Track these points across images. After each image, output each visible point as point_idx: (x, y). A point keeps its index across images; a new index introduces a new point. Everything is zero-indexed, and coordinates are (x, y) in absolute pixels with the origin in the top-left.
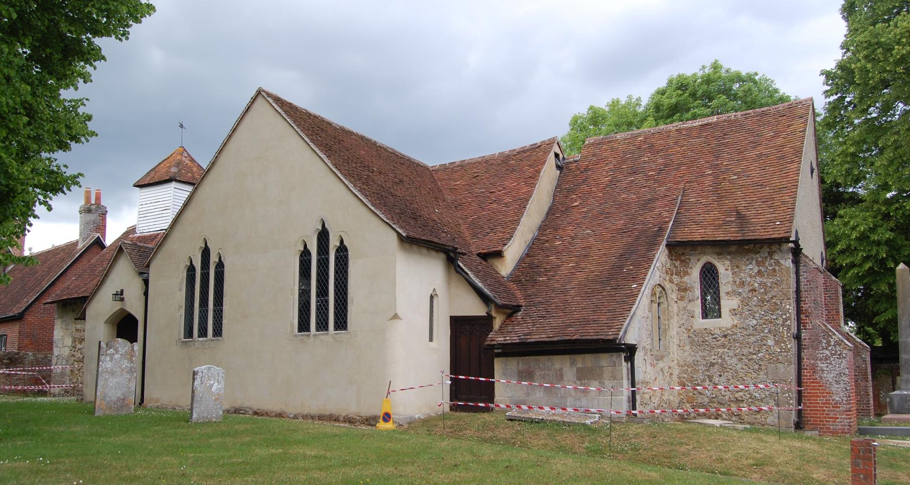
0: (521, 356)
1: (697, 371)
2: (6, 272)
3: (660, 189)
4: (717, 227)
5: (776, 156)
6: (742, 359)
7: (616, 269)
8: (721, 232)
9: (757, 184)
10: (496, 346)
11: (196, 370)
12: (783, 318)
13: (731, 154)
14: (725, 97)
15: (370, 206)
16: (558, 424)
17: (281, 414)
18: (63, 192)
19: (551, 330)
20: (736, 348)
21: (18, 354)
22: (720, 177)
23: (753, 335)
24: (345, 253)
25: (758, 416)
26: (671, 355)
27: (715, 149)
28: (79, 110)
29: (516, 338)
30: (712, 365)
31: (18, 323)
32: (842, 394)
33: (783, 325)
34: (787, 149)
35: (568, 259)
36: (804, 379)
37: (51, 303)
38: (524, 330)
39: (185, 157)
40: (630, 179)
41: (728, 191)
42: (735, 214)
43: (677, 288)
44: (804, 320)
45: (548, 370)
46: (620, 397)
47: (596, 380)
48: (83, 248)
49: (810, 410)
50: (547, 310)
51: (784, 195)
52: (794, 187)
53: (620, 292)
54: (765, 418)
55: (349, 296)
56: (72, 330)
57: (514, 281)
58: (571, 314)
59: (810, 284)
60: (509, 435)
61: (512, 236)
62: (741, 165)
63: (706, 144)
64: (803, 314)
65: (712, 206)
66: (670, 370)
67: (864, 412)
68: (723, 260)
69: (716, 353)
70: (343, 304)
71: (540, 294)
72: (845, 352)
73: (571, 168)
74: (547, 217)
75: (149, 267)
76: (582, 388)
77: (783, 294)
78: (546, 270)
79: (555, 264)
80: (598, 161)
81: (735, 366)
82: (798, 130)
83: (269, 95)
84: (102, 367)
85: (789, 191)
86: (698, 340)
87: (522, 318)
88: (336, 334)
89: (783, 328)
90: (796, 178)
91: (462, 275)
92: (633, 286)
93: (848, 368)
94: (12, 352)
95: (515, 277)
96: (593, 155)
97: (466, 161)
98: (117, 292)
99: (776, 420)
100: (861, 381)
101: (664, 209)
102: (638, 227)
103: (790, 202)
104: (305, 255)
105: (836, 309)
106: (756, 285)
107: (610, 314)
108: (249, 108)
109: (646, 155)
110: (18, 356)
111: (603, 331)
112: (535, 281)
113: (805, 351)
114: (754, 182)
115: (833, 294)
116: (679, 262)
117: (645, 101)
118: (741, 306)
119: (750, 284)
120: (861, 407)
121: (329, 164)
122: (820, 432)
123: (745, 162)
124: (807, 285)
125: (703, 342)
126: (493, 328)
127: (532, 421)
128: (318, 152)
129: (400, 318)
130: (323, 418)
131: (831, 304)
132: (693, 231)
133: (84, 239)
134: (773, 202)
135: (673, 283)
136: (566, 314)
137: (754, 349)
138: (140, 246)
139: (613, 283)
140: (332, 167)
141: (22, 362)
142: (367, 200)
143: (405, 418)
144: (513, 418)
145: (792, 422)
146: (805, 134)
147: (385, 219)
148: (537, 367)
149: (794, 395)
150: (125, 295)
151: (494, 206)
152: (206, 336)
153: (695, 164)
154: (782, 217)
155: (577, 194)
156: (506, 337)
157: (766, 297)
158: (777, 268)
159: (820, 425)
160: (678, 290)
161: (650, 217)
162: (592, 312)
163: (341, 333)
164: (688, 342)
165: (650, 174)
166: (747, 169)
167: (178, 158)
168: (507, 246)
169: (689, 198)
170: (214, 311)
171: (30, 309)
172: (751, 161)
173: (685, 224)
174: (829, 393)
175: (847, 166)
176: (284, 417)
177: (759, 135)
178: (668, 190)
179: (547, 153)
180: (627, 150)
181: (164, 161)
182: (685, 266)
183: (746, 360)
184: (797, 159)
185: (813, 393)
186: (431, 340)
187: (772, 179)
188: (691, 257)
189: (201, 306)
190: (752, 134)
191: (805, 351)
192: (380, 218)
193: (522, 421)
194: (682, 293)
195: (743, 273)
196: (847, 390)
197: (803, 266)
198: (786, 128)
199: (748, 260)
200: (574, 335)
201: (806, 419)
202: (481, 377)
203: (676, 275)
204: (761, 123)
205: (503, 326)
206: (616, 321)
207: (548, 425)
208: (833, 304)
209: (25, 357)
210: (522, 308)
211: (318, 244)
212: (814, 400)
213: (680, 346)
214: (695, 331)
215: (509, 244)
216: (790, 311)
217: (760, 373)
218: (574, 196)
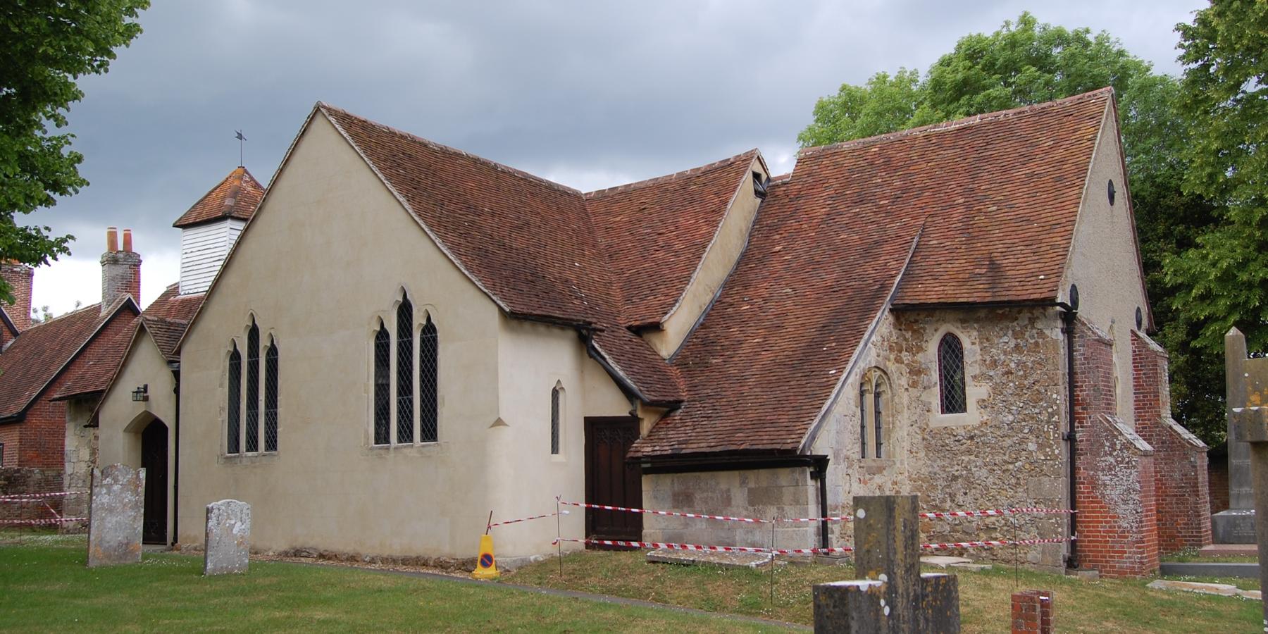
0: (677, 473)
1: (934, 487)
3: (892, 225)
5: (1052, 176)
6: (994, 471)
7: (815, 345)
8: (965, 291)
9: (1022, 219)
10: (642, 459)
11: (210, 506)
12: (1048, 412)
13: (993, 174)
14: (1034, 69)
15: (463, 270)
16: (713, 567)
17: (354, 557)
18: (46, 263)
19: (714, 437)
20: (987, 454)
21: (18, 471)
22: (974, 209)
23: (1009, 436)
24: (434, 335)
26: (898, 464)
27: (973, 166)
28: (62, 151)
29: (667, 448)
30: (955, 478)
31: (18, 427)
32: (1131, 518)
33: (1048, 422)
34: (1068, 166)
35: (755, 331)
36: (1081, 498)
37: (60, 399)
38: (680, 435)
39: (246, 182)
40: (854, 211)
41: (983, 229)
42: (988, 263)
43: (908, 370)
44: (1081, 413)
45: (711, 492)
46: (805, 529)
47: (774, 505)
48: (108, 316)
49: (1088, 540)
50: (715, 408)
51: (1056, 235)
52: (1070, 223)
53: (813, 381)
54: (1025, 553)
55: (439, 395)
56: (89, 438)
57: (679, 365)
58: (745, 412)
59: (1088, 363)
60: (644, 584)
61: (676, 301)
62: (1005, 190)
63: (962, 158)
64: (1079, 405)
65: (958, 251)
66: (895, 487)
67: (1193, 540)
69: (960, 462)
70: (431, 405)
71: (710, 384)
72: (1135, 459)
73: (777, 194)
74: (736, 269)
76: (735, 519)
77: (1048, 378)
78: (724, 347)
79: (737, 339)
80: (814, 183)
81: (985, 480)
82: (1085, 138)
83: (329, 110)
84: (96, 503)
85: (1063, 229)
86: (936, 444)
87: (681, 419)
88: (423, 446)
89: (1048, 426)
90: (1075, 209)
91: (597, 360)
92: (830, 372)
93: (1139, 482)
94: (10, 468)
95: (680, 360)
96: (809, 175)
97: (632, 186)
98: (138, 388)
99: (1040, 556)
100: (1189, 495)
101: (892, 257)
102: (854, 283)
103: (1062, 246)
104: (382, 337)
105: (1154, 392)
106: (1013, 365)
107: (794, 412)
108: (305, 130)
109: (879, 174)
110: (18, 474)
111: (780, 437)
112: (707, 365)
113: (1082, 458)
114: (1018, 216)
115: (1151, 369)
116: (910, 333)
117: (923, 77)
118: (992, 395)
119: (1005, 364)
120: (1189, 532)
121: (410, 211)
122: (1101, 572)
123: (1010, 186)
124: (1084, 364)
125: (943, 446)
126: (640, 434)
127: (680, 563)
128: (396, 193)
129: (505, 424)
130: (408, 562)
131: (1147, 385)
132: (928, 289)
133: (109, 303)
134: (1039, 245)
135: (902, 363)
136: (738, 413)
137: (1010, 457)
138: (169, 323)
139: (806, 367)
140: (413, 214)
141: (24, 483)
142: (459, 262)
143: (514, 561)
144: (656, 560)
145: (1061, 558)
146: (1094, 143)
147: (482, 288)
148: (697, 487)
149: (1066, 520)
151: (661, 254)
152: (257, 450)
153: (943, 188)
154: (1048, 268)
155: (781, 234)
156: (655, 446)
157: (1026, 382)
158: (1040, 341)
159: (1102, 561)
160: (909, 373)
161: (871, 270)
162: (772, 410)
163: (430, 445)
164: (922, 446)
165: (881, 203)
166: (1011, 196)
167: (235, 183)
169: (929, 239)
170: (267, 414)
172: (1019, 184)
173: (919, 279)
174: (1114, 517)
175: (1208, 170)
176: (358, 561)
178: (902, 228)
179: (740, 173)
180: (854, 167)
181: (216, 189)
182: (918, 338)
183: (999, 472)
184: (1078, 182)
185: (1093, 517)
186: (555, 449)
187: (1043, 212)
188: (926, 326)
189: (249, 407)
190: (1024, 143)
191: (1082, 458)
192: (477, 286)
193: (668, 563)
194: (915, 377)
195: (995, 348)
196: (1137, 512)
197: (1079, 337)
198: (1071, 135)
199: (1001, 329)
200: (742, 444)
201: (1083, 554)
202: (607, 505)
203: (906, 351)
204: (1038, 127)
205: (655, 430)
206: (799, 424)
207: (699, 569)
208: (1151, 385)
209: (29, 475)
210: (682, 404)
212: (1093, 527)
213: (912, 453)
214: (931, 431)
215: (672, 312)
216: (1058, 402)
217: (1019, 490)
218: (777, 237)
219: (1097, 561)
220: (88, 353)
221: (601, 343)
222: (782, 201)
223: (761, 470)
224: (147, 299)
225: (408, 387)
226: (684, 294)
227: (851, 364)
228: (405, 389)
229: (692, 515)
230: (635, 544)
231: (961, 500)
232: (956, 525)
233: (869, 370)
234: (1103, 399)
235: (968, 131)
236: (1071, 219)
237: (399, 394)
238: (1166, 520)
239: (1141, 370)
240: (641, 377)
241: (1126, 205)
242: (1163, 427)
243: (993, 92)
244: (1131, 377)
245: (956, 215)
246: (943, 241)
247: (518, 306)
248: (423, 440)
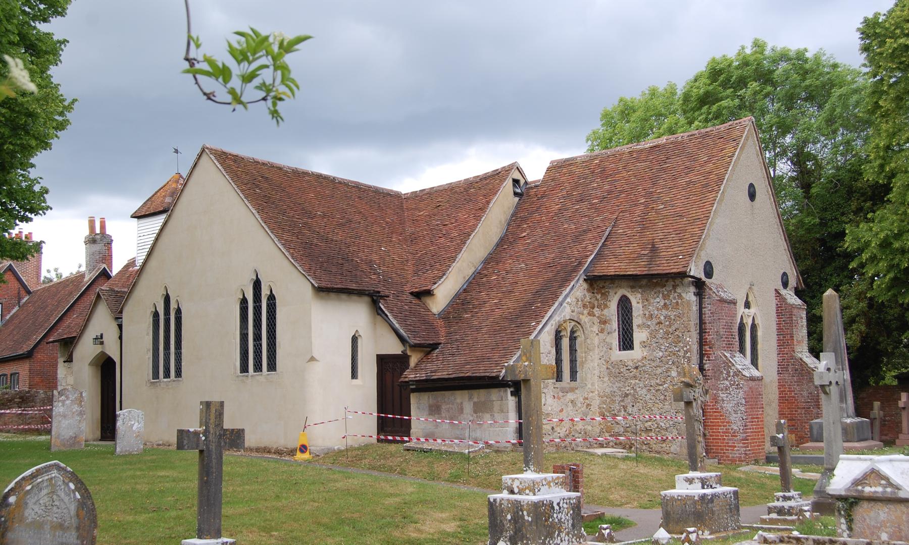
0: (434, 391)
1: (614, 401)
2: (21, 304)
4: (631, 261)
8: (632, 266)
15: (291, 259)
16: (440, 452)
18: (27, 259)
21: (28, 392)
25: (664, 445)
26: (589, 386)
30: (627, 395)
37: (54, 342)
40: (576, 207)
41: (652, 222)
42: (650, 246)
51: (696, 226)
52: (706, 218)
59: (713, 316)
61: (444, 274)
68: (635, 293)
75: (122, 313)
85: (700, 223)
88: (268, 375)
95: (445, 315)
96: (553, 180)
99: (678, 449)
100: (813, 408)
104: (244, 302)
105: (790, 334)
106: (662, 318)
108: (196, 164)
113: (709, 381)
115: (788, 318)
116: (600, 295)
124: (710, 317)
127: (425, 451)
128: (250, 207)
129: (315, 360)
132: (610, 265)
133: (90, 271)
135: (595, 316)
138: (117, 291)
141: (33, 401)
150: (104, 339)
158: (680, 301)
163: (272, 374)
168: (436, 285)
170: (176, 354)
171: (40, 347)
177: (695, 159)
178: (602, 221)
179: (502, 181)
181: (160, 190)
186: (354, 375)
191: (709, 381)
196: (743, 419)
199: (655, 293)
208: (788, 329)
211: (253, 292)
212: (716, 429)
215: (440, 282)
217: (666, 403)
218: (525, 226)
219: (718, 453)
220: (76, 308)
221: (386, 305)
222: (532, 200)
223: (481, 390)
224: (117, 267)
225: (259, 336)
226: (450, 270)
227: (546, 318)
228: (257, 338)
229: (440, 421)
230: (406, 439)
231: (630, 410)
232: (627, 427)
233: (565, 321)
234: (724, 341)
235: (657, 149)
236: (707, 215)
237: (254, 340)
238: (798, 426)
239: (782, 318)
240: (412, 328)
241: (770, 199)
242: (796, 359)
243: (724, 103)
244: (775, 323)
245: (638, 211)
246: (626, 230)
247: (324, 283)
248: (268, 371)
